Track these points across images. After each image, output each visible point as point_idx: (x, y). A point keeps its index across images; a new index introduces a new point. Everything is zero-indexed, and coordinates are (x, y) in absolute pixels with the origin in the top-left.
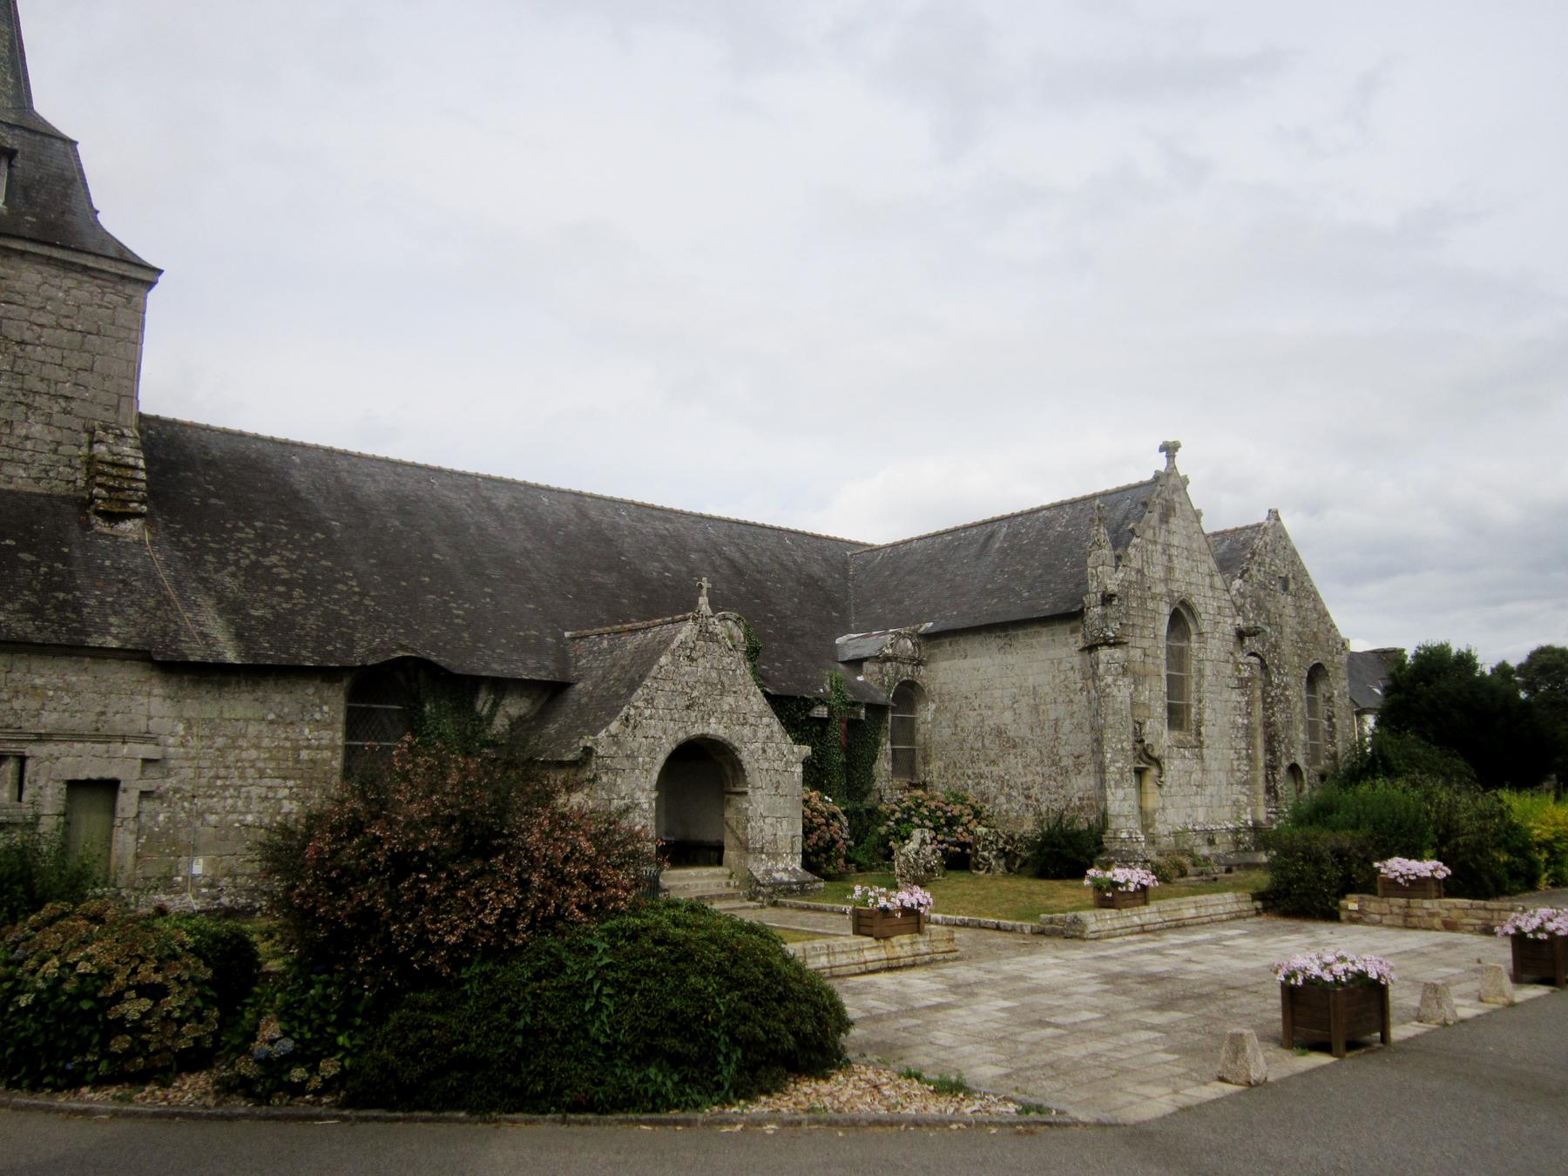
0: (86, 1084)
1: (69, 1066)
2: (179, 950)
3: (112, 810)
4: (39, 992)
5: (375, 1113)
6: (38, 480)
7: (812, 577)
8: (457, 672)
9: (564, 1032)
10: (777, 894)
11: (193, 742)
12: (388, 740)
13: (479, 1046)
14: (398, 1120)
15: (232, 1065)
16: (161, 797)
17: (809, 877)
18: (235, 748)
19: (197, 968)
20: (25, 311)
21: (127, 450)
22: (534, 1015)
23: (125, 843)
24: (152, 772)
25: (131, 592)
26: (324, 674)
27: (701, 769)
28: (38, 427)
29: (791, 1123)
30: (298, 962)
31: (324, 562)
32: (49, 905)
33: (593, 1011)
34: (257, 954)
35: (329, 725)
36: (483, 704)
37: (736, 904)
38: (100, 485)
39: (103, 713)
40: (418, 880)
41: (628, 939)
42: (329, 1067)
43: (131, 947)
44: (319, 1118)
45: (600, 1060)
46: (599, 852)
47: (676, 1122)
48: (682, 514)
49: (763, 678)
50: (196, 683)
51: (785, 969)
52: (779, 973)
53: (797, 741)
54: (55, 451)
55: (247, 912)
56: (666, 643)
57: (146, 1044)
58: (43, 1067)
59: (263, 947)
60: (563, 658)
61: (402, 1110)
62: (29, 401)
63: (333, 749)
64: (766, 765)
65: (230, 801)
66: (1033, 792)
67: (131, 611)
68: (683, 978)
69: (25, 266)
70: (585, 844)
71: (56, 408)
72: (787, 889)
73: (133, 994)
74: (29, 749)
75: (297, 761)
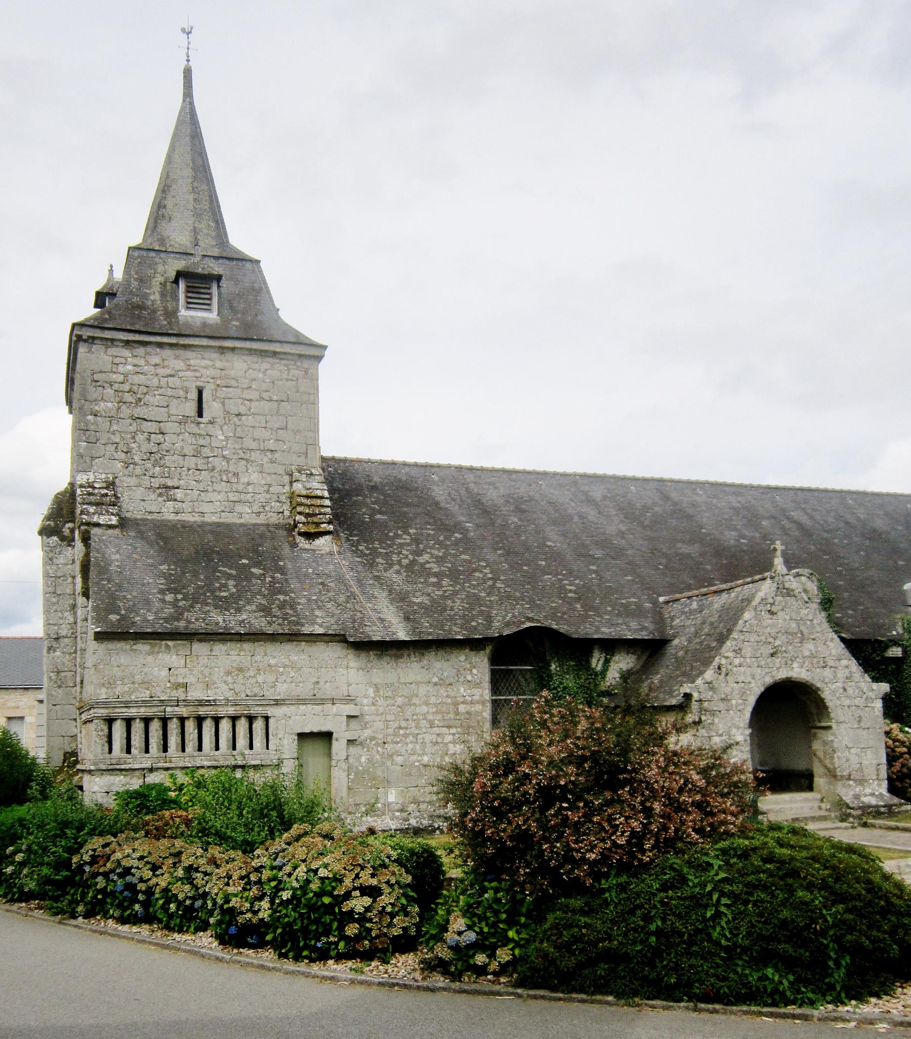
0: (331, 958)
1: (319, 945)
2: (387, 860)
3: (329, 755)
4: (293, 889)
5: (542, 992)
6: (258, 514)
7: (875, 531)
8: (574, 636)
9: (690, 935)
10: (867, 815)
11: (381, 702)
12: (524, 694)
13: (620, 943)
14: (560, 999)
15: (431, 949)
16: (361, 744)
17: (896, 800)
18: (410, 705)
19: (401, 875)
20: (239, 391)
21: (315, 485)
22: (664, 920)
23: (340, 778)
24: (354, 724)
25: (328, 591)
26: (473, 644)
27: (788, 708)
28: (255, 475)
29: (901, 1024)
30: (474, 871)
31: (463, 557)
32: (295, 826)
33: (713, 917)
34: (441, 865)
35: (478, 685)
36: (597, 661)
37: (828, 824)
38: (300, 513)
39: (318, 682)
40: (561, 808)
41: (739, 857)
42: (504, 955)
43: (354, 858)
44: (499, 994)
45: (722, 958)
46: (708, 783)
47: (794, 1016)
48: (752, 487)
49: (837, 625)
50: (380, 657)
51: (886, 886)
52: (880, 889)
53: (875, 679)
54: (268, 492)
55: (430, 831)
56: (748, 601)
57: (369, 930)
58: (302, 944)
59: (445, 860)
60: (660, 620)
61: (563, 992)
62: (247, 456)
63: (483, 703)
64: (847, 702)
65: (410, 746)
67: (329, 605)
68: (791, 891)
69: (236, 358)
70: (696, 777)
71: (266, 460)
72: (877, 813)
73: (357, 893)
74: (270, 711)
75: (457, 713)
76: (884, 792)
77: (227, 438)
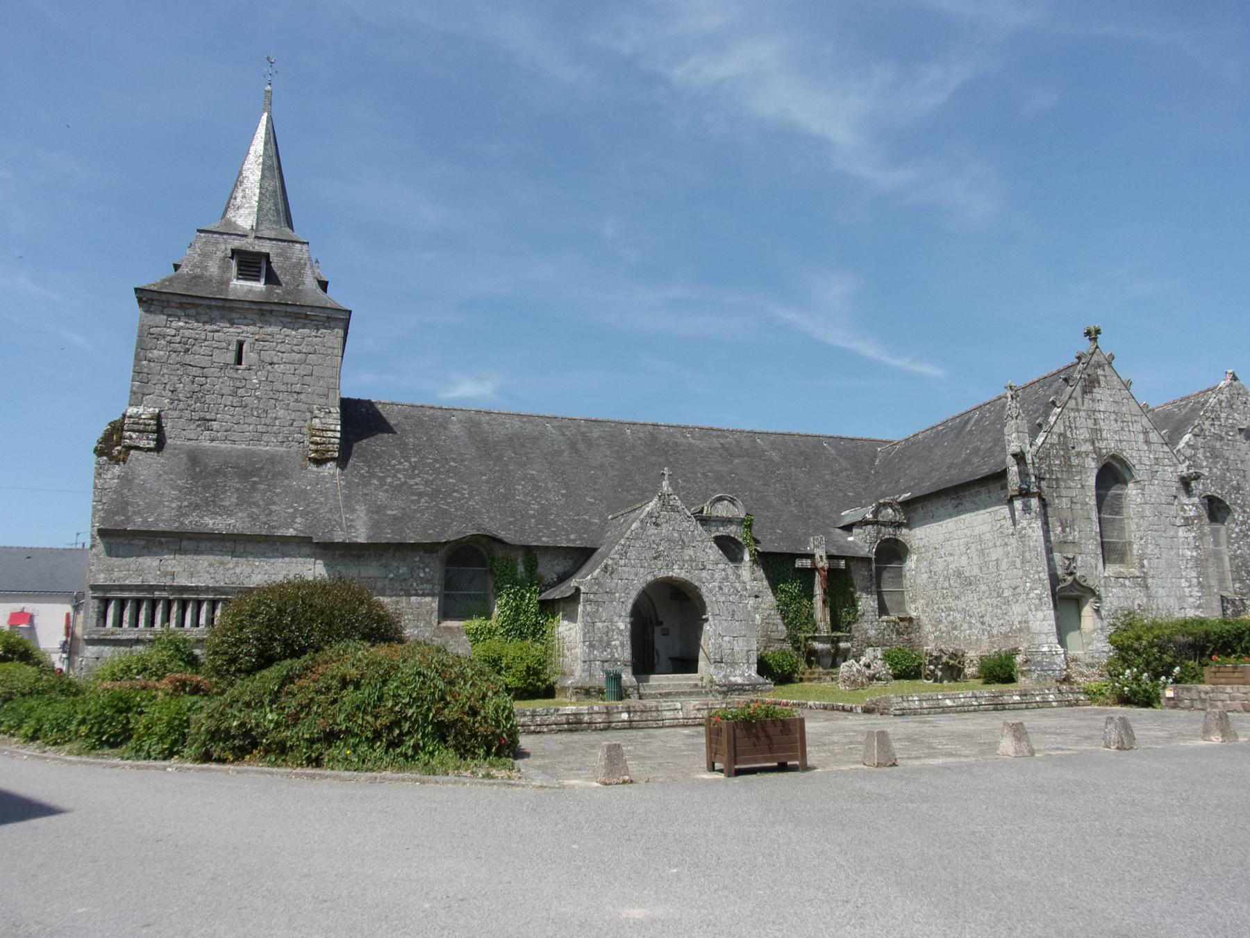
17: (761, 680)
21: (330, 421)
66: (987, 619)
76: (754, 674)
77: (260, 382)
